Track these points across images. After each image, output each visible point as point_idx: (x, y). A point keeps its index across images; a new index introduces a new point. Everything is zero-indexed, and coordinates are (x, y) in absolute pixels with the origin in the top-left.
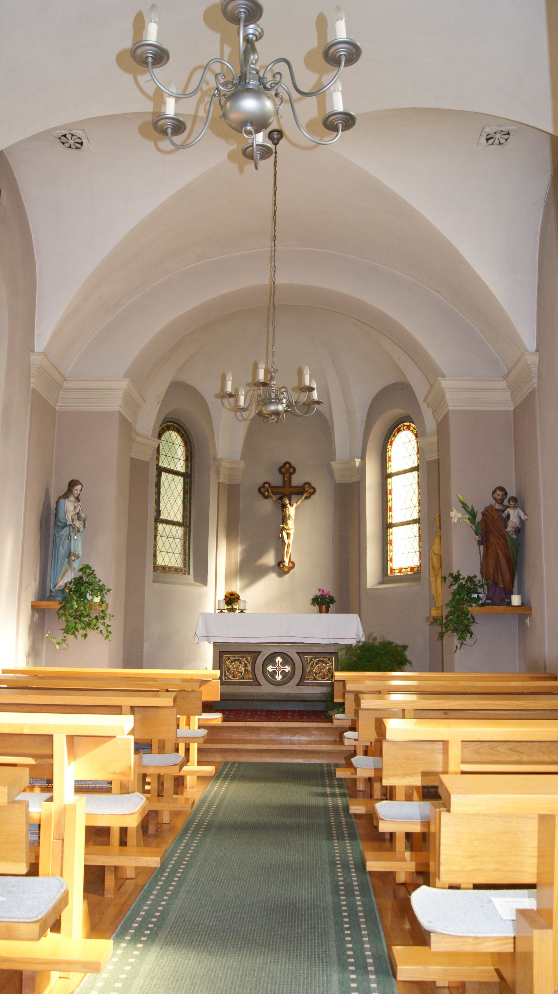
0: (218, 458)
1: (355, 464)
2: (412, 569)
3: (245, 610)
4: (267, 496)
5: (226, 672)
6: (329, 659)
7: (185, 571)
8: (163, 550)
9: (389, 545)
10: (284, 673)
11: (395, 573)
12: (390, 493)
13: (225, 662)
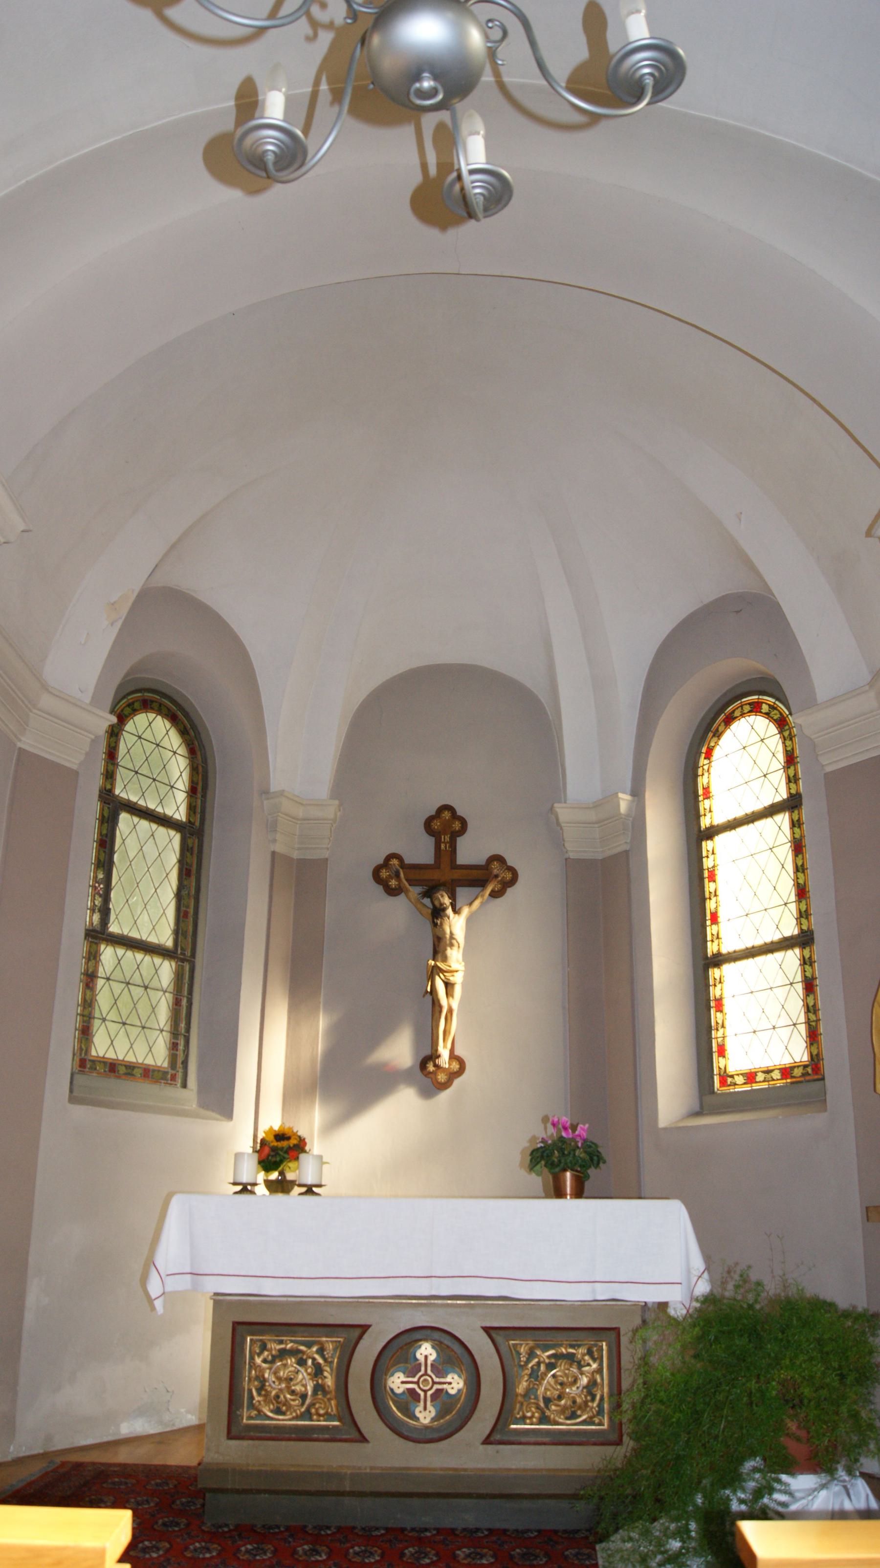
0: (272, 790)
1: (619, 806)
2: (786, 1072)
3: (319, 1186)
4: (395, 889)
5: (255, 1393)
6: (590, 1353)
7: (173, 1078)
8: (112, 1016)
9: (713, 1011)
10: (443, 1396)
11: (735, 1084)
12: (712, 878)
13: (252, 1358)
